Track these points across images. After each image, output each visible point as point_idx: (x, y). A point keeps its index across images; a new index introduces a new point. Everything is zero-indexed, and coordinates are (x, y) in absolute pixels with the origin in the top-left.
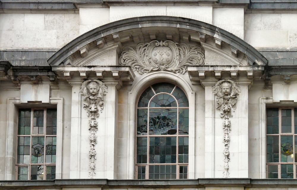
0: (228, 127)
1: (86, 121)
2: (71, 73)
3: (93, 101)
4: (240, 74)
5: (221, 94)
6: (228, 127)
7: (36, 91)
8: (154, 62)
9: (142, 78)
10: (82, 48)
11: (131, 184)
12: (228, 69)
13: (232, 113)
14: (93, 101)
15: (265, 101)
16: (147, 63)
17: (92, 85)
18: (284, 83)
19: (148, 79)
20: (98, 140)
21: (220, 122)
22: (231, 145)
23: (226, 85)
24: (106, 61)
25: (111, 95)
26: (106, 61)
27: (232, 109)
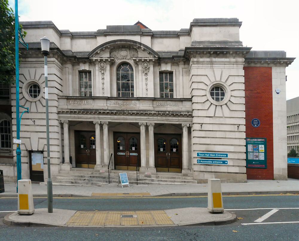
4: (150, 60)
7: (85, 66)
8: (122, 56)
9: (118, 62)
12: (146, 58)
13: (148, 74)
16: (119, 56)
17: (102, 64)
19: (120, 62)
21: (144, 77)
23: (145, 64)
25: (108, 68)
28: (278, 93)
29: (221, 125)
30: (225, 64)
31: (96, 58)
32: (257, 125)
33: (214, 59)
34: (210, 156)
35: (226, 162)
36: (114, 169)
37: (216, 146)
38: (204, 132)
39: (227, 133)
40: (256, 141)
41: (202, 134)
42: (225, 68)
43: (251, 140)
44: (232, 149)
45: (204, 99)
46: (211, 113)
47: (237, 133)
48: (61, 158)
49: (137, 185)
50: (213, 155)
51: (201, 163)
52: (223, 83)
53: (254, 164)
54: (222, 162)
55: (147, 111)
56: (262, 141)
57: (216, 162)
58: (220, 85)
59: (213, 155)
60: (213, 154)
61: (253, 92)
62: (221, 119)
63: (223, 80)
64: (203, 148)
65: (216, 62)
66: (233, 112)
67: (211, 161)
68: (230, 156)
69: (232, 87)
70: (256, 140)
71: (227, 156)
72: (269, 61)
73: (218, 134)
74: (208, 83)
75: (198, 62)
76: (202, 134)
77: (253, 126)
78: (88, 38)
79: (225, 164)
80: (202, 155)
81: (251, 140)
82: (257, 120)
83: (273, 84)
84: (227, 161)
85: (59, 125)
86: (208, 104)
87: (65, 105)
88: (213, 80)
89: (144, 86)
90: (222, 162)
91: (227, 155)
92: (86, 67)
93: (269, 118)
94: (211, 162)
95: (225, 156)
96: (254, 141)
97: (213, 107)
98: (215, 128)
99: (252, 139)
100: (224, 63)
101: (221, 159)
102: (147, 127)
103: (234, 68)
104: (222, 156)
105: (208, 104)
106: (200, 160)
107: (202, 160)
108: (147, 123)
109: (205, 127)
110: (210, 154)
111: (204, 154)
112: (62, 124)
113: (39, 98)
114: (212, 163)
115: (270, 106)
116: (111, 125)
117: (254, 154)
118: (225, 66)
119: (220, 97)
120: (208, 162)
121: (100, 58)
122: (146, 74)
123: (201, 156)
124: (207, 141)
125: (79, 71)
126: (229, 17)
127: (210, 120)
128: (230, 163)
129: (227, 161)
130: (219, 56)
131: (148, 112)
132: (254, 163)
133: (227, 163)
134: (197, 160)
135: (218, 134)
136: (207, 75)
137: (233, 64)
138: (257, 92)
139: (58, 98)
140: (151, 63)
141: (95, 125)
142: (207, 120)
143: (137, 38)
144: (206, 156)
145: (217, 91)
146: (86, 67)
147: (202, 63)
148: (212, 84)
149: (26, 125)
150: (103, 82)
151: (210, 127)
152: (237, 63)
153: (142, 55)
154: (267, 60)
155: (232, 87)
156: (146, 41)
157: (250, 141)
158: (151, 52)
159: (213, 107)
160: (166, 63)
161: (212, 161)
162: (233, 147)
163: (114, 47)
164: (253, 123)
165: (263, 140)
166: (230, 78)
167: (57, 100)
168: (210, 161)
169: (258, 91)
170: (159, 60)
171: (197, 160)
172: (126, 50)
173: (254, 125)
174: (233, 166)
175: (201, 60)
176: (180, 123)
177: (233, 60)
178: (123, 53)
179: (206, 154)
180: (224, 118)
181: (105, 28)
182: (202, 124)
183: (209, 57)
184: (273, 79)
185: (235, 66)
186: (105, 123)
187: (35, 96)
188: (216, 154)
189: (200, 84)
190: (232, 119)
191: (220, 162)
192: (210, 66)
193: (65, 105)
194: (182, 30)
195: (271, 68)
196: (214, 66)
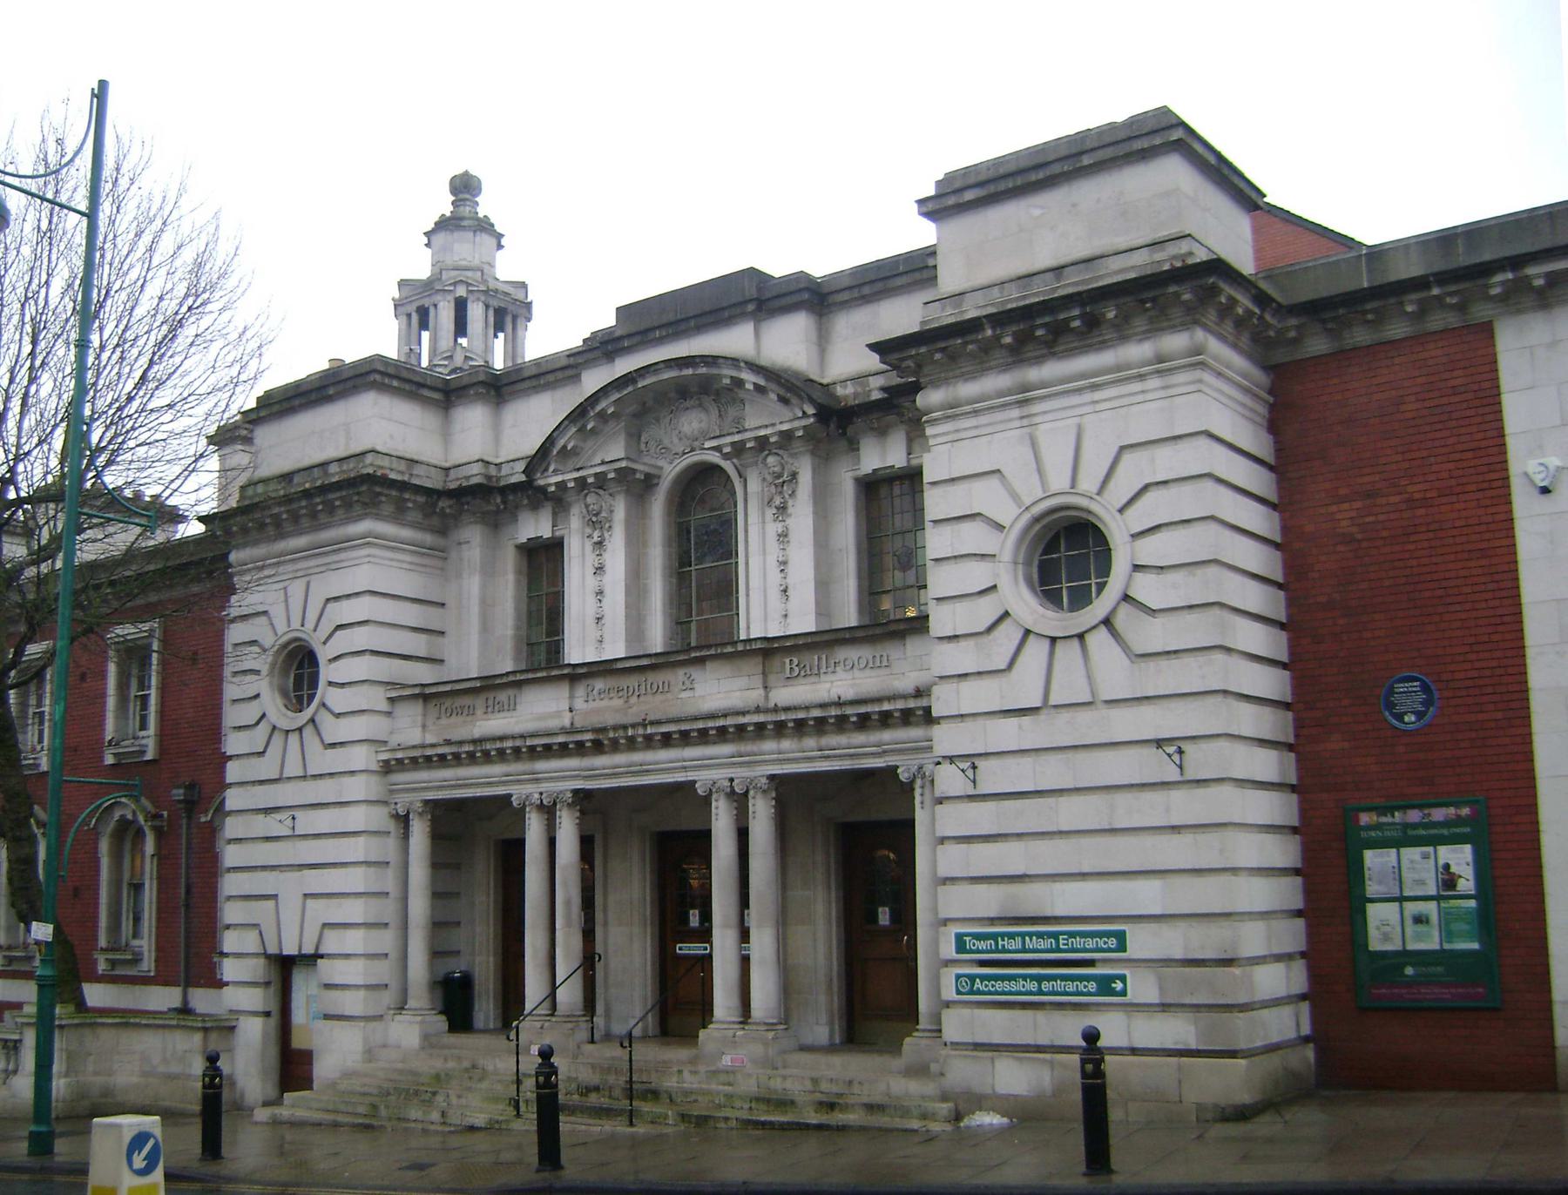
0: (783, 536)
1: (591, 560)
2: (1548, 275)
3: (597, 522)
4: (787, 436)
5: (769, 478)
6: (783, 536)
7: (537, 521)
8: (688, 439)
9: (670, 470)
10: (1073, 318)
11: (661, 660)
12: (762, 433)
13: (790, 510)
14: (597, 522)
15: (850, 474)
16: (676, 440)
17: (589, 500)
18: (1239, 361)
19: (678, 469)
20: (607, 591)
21: (773, 528)
22: (790, 569)
23: (771, 460)
24: (613, 450)
25: (620, 509)
26: (613, 450)
27: (790, 503)
28: (1545, 491)
29: (1081, 756)
30: (1095, 387)
31: (559, 478)
32: (1420, 715)
33: (1034, 374)
34: (1024, 950)
35: (1118, 986)
36: (657, 1031)
37: (1058, 887)
38: (990, 805)
39: (1121, 799)
40: (1415, 826)
41: (982, 817)
42: (1099, 407)
43: (1384, 819)
44: (1147, 896)
45: (986, 611)
46: (1025, 687)
47: (1177, 795)
48: (394, 985)
49: (631, 1124)
50: (1042, 944)
51: (979, 992)
52: (1084, 502)
53: (1410, 983)
54: (1092, 986)
55: (725, 716)
56: (1459, 821)
57: (1059, 985)
58: (1056, 516)
59: (1042, 944)
60: (1040, 935)
61: (1383, 501)
62: (1084, 716)
63: (1088, 484)
64: (988, 901)
65: (1043, 385)
66: (1152, 665)
67: (1033, 978)
68: (1141, 943)
69: (1140, 517)
70: (1414, 816)
71: (1122, 947)
72: (1451, 294)
73: (1070, 813)
74: (1006, 512)
75: (953, 410)
76: (982, 817)
77: (1394, 722)
78: (557, 381)
79: (1113, 993)
80: (982, 945)
81: (1384, 819)
82: (1416, 679)
83: (1510, 428)
84: (1123, 978)
85: (391, 825)
86: (1007, 637)
87: (411, 729)
88: (1030, 491)
89: (774, 577)
90: (1092, 986)
91: (1121, 936)
92: (535, 526)
93: (1498, 654)
94: (1033, 986)
95: (1112, 943)
96: (1406, 826)
97: (1036, 652)
98: (1051, 772)
99: (1390, 810)
100: (1091, 383)
101: (983, 963)
102: (740, 801)
103: (963, 435)
104: (1090, 943)
105: (1007, 637)
106: (972, 978)
107: (983, 978)
108: (732, 780)
109: (994, 777)
110: (1023, 935)
111: (994, 937)
112: (403, 820)
113: (1100, 607)
114: (1040, 992)
115: (1497, 577)
116: (787, 790)
117: (1407, 914)
118: (1098, 395)
119: (1093, 581)
120: (1013, 986)
121: (576, 475)
122: (782, 509)
123: (978, 951)
124: (1010, 858)
125: (520, 547)
126: (1120, 115)
127: (1020, 727)
128: (1142, 988)
129: (1123, 978)
130: (1062, 348)
131: (729, 721)
132: (1409, 971)
133: (1123, 993)
134: (958, 977)
135: (1070, 813)
136: (1122, 448)
137: (1141, 377)
138: (1408, 501)
139: (391, 700)
140: (798, 446)
141: (706, 801)
142: (1008, 734)
143: (735, 340)
144: (1004, 951)
145: (1067, 551)
146: (535, 526)
147: (968, 408)
148: (1027, 517)
149: (268, 839)
150: (609, 594)
151: (1019, 775)
152: (1196, 360)
153: (766, 418)
154: (1436, 291)
155: (1140, 517)
156: (786, 342)
157: (1378, 827)
158: (788, 385)
159: (1036, 652)
160: (882, 432)
161: (1039, 979)
162: (1155, 884)
163: (642, 404)
164: (1390, 706)
165: (1465, 811)
166: (1127, 458)
167: (384, 706)
168: (1024, 977)
169: (1410, 489)
170: (836, 421)
171: (958, 977)
172: (700, 405)
173: (1400, 717)
174: (1164, 1007)
175: (967, 389)
176: (890, 760)
177: (1136, 351)
178: (692, 422)
179: (1003, 935)
180: (1100, 705)
181: (609, 320)
182: (972, 760)
183: (1006, 367)
184: (1506, 400)
185: (1154, 383)
186: (750, 785)
187: (1081, 599)
188: (1055, 935)
189: (966, 527)
190: (1146, 710)
191: (1081, 987)
192: (1015, 413)
193: (411, 729)
194: (624, 312)
195: (1486, 332)
196: (1037, 408)
